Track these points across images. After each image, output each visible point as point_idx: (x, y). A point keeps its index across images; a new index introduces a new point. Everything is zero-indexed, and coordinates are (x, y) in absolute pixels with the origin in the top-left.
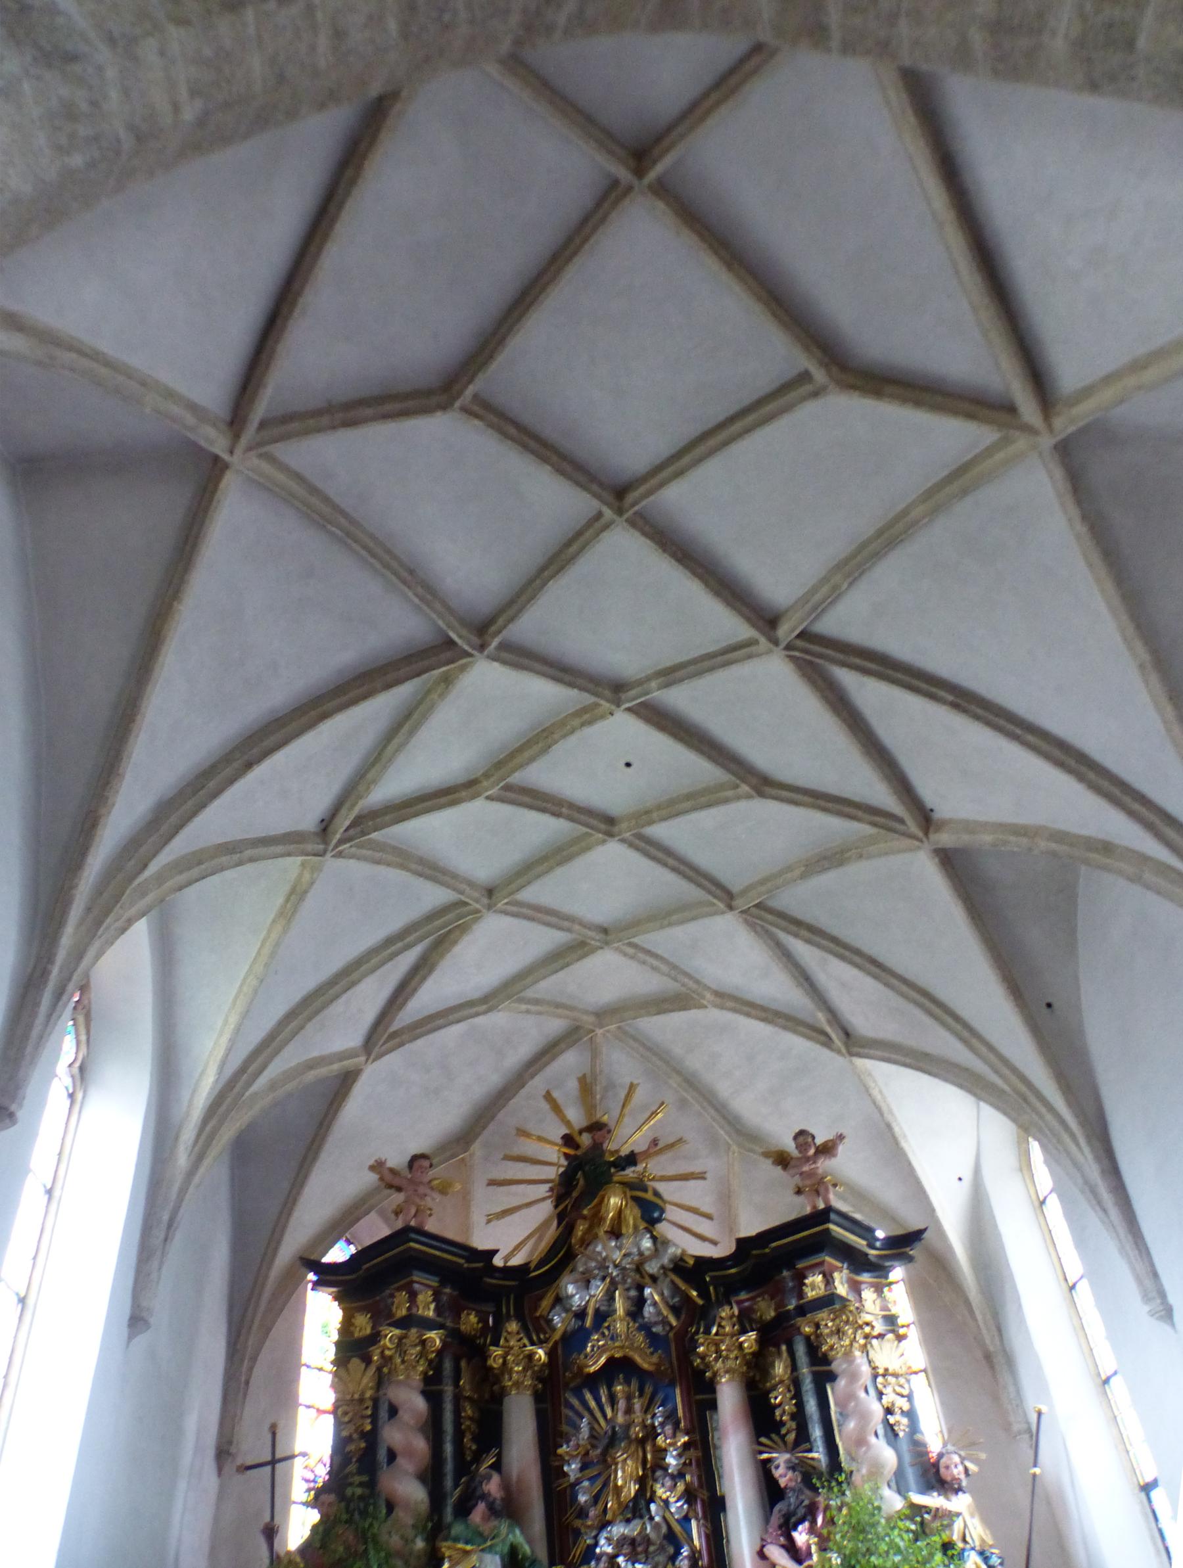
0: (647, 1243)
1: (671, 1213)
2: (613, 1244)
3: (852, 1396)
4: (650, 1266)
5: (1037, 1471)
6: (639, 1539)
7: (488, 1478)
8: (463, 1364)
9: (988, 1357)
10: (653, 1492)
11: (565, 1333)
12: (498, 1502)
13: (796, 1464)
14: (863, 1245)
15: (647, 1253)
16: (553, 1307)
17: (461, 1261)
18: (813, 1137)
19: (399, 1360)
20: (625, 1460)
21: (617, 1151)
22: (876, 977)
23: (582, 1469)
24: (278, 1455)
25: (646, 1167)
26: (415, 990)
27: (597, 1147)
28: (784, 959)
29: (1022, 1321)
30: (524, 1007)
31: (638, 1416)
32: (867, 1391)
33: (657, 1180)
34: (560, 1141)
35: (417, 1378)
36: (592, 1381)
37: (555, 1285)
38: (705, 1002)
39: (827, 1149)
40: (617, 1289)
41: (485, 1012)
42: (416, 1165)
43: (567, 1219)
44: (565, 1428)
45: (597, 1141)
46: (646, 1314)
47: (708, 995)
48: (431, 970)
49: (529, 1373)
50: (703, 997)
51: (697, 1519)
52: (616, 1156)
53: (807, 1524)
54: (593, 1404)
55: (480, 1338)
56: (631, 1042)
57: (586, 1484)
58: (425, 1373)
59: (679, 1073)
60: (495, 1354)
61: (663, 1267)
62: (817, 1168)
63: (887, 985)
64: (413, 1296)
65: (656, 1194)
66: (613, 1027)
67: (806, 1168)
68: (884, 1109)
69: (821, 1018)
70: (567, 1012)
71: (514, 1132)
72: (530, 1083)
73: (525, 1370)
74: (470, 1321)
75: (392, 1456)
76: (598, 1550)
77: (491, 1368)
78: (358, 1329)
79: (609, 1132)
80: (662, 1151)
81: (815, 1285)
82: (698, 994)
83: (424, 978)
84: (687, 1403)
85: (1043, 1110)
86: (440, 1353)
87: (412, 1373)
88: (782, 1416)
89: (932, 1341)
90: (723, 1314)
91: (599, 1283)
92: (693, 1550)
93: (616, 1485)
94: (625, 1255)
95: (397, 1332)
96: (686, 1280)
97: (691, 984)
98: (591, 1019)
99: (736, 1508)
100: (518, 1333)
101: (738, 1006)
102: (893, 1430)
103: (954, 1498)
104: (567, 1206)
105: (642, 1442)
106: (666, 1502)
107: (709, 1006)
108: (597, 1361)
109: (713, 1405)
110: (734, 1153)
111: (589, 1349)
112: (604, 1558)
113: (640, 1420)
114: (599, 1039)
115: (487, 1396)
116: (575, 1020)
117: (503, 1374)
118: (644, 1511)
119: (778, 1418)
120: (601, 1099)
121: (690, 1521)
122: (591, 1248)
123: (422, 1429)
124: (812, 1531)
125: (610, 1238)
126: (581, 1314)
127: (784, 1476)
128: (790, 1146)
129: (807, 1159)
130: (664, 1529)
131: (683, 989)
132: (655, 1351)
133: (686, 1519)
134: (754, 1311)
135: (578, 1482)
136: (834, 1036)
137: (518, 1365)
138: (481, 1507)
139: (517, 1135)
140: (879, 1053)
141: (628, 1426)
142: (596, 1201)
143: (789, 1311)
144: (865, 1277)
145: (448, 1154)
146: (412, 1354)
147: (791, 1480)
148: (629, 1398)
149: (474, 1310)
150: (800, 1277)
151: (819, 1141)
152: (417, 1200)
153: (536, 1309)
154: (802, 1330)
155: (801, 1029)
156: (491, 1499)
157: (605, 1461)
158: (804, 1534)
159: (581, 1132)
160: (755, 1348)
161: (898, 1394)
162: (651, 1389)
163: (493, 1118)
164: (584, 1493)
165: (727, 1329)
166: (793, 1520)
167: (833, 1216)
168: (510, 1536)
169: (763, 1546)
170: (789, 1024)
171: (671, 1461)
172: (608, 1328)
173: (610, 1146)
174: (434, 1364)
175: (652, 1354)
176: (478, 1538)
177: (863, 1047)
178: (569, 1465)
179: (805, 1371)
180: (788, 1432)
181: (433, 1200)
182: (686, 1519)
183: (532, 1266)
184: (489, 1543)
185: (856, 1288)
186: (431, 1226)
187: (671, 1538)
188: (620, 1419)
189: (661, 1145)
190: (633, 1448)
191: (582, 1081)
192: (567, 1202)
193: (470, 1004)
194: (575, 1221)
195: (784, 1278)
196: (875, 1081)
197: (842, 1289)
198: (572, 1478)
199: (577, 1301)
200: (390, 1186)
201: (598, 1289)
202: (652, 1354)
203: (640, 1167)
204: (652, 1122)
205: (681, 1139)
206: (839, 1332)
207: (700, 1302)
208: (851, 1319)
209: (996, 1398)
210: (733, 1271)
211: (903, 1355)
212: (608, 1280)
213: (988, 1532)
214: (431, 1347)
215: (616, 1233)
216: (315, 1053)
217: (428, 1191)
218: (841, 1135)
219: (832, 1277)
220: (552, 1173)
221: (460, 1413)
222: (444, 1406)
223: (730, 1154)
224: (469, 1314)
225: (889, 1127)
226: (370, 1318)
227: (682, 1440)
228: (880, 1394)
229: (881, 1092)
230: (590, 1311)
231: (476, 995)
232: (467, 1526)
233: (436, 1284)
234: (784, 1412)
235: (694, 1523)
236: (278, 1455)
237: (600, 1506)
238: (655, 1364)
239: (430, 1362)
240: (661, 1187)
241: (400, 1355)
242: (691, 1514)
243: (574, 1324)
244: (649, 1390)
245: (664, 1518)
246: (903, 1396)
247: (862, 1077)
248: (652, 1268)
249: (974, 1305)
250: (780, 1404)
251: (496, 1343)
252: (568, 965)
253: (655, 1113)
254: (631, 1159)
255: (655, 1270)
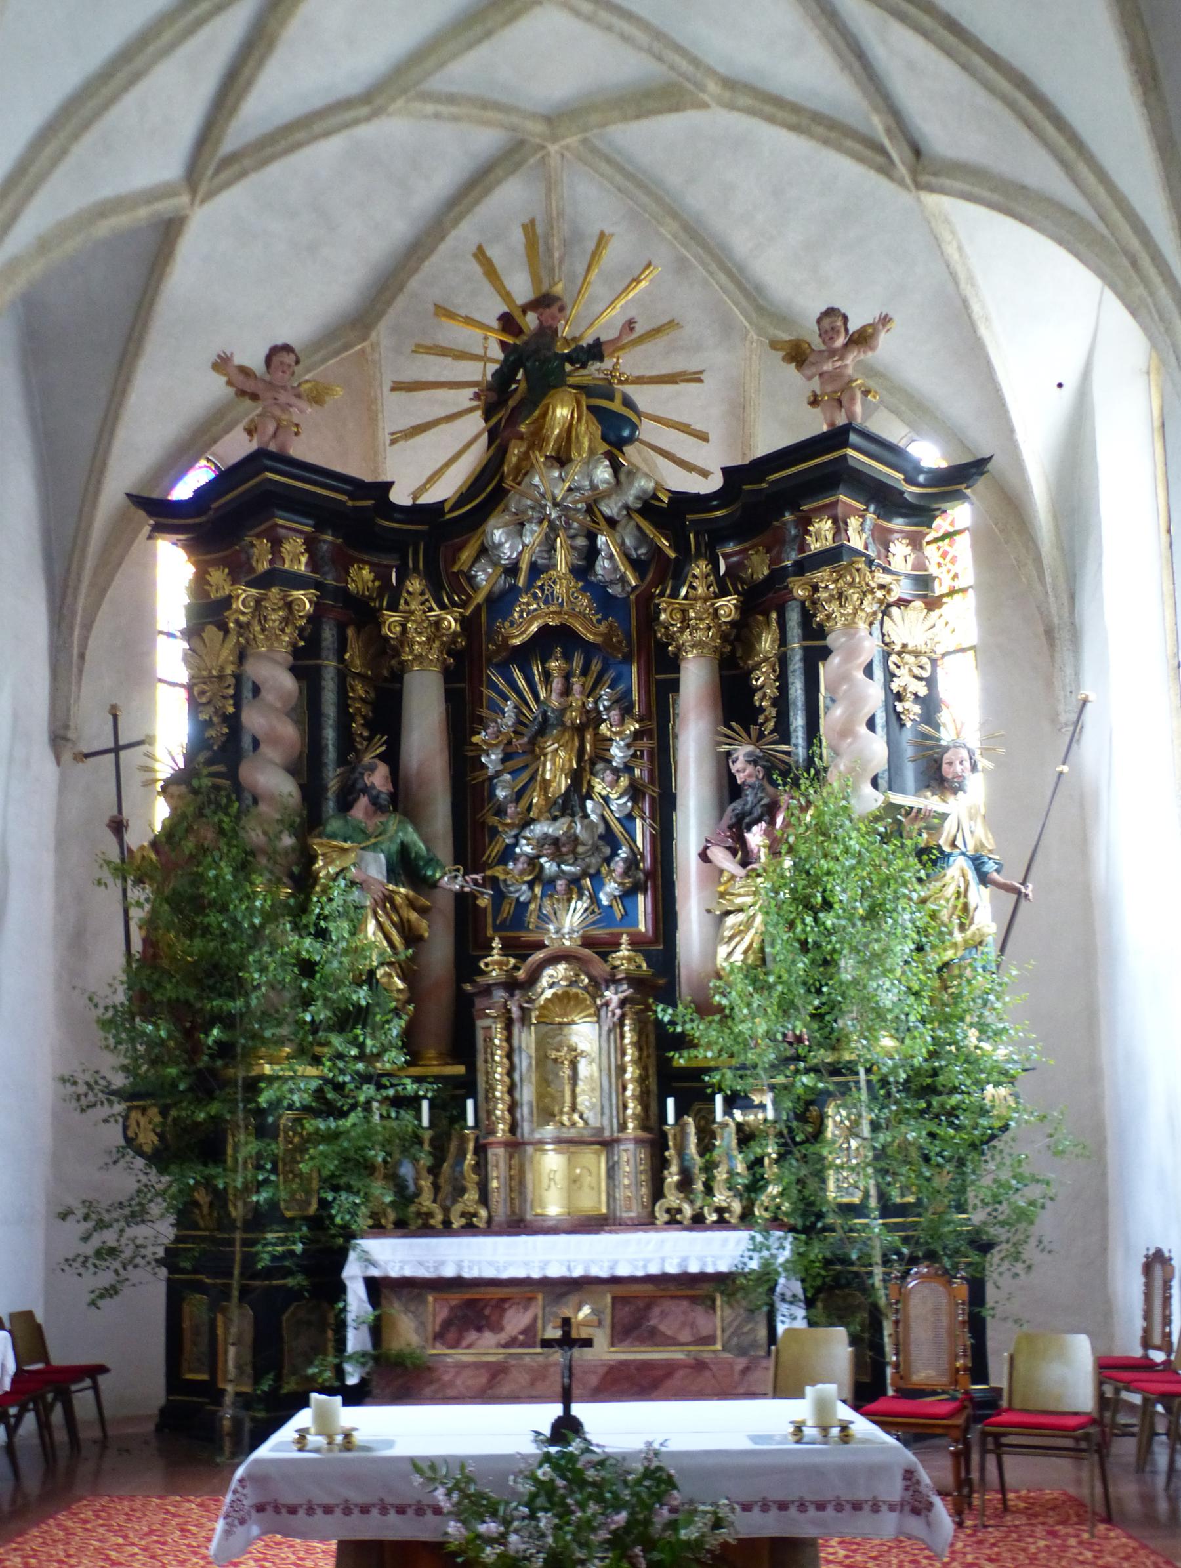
0: (603, 473)
1: (648, 430)
2: (556, 474)
3: (846, 677)
4: (608, 506)
5: (1065, 769)
6: (564, 839)
7: (372, 769)
8: (350, 632)
9: (1050, 633)
10: (591, 787)
11: (490, 593)
12: (383, 796)
13: (759, 757)
14: (898, 480)
15: (603, 487)
16: (476, 559)
17: (343, 498)
18: (845, 319)
19: (258, 628)
20: (557, 750)
21: (574, 339)
22: (949, 52)
23: (503, 761)
24: (122, 742)
25: (617, 363)
26: (249, 83)
27: (547, 333)
28: (823, 21)
29: (1098, 585)
30: (430, 108)
31: (576, 699)
32: (869, 671)
33: (633, 383)
34: (495, 324)
35: (282, 648)
36: (524, 655)
37: (480, 530)
38: (706, 97)
39: (862, 339)
40: (558, 536)
41: (368, 119)
42: (276, 360)
43: (498, 441)
44: (485, 712)
45: (545, 324)
46: (599, 570)
47: (712, 86)
48: (271, 45)
49: (437, 644)
50: (702, 88)
51: (643, 819)
52: (573, 346)
53: (763, 825)
54: (522, 683)
55: (374, 600)
56: (604, 167)
57: (507, 777)
58: (294, 645)
59: (675, 215)
60: (392, 619)
61: (626, 507)
62: (846, 366)
63: (965, 67)
64: (276, 544)
65: (628, 402)
66: (572, 140)
67: (828, 367)
68: (962, 276)
69: (877, 125)
70: (499, 116)
71: (431, 308)
72: (454, 233)
73: (430, 640)
74: (362, 578)
75: (256, 744)
76: (518, 850)
77: (387, 639)
78: (214, 588)
79: (562, 309)
80: (642, 339)
81: (821, 535)
82: (695, 84)
83: (260, 64)
84: (645, 685)
85: (1157, 280)
86: (315, 619)
87: (276, 645)
88: (761, 701)
89: (988, 612)
90: (697, 572)
91: (536, 528)
92: (633, 850)
93: (544, 780)
94: (570, 490)
95: (253, 592)
96: (659, 526)
97: (684, 65)
98: (538, 127)
99: (687, 807)
100: (422, 593)
101: (757, 105)
102: (899, 719)
103: (951, 799)
104: (500, 420)
105: (580, 730)
106: (606, 799)
107: (713, 104)
108: (526, 630)
109: (674, 686)
110: (752, 343)
111: (516, 615)
112: (522, 859)
113: (580, 703)
114: (555, 161)
115: (385, 673)
116: (514, 129)
117: (402, 645)
118: (578, 809)
119: (757, 703)
120: (561, 261)
121: (635, 819)
122: (527, 479)
123: (292, 713)
124: (768, 833)
125: (552, 467)
126: (512, 570)
127: (742, 770)
128: (811, 335)
129: (832, 353)
130: (601, 829)
131: (673, 76)
132: (605, 618)
133: (630, 817)
134: (745, 568)
135: (498, 774)
136: (895, 156)
137: (420, 634)
138: (364, 801)
139: (436, 314)
140: (958, 185)
141: (562, 711)
142: (537, 413)
143: (786, 567)
144: (898, 524)
145: (339, 344)
146: (274, 621)
147: (750, 776)
148: (567, 677)
149: (366, 562)
150: (805, 522)
151: (853, 327)
152: (278, 412)
153: (454, 561)
154: (795, 594)
155: (849, 143)
156: (374, 792)
157: (533, 751)
158: (758, 836)
159: (524, 310)
160: (734, 615)
161: (916, 677)
162: (599, 666)
163: (401, 288)
164: (503, 788)
165: (700, 591)
166: (747, 820)
167: (853, 438)
168: (400, 834)
169: (706, 848)
170: (833, 135)
171: (617, 753)
172: (541, 588)
173: (565, 331)
174: (306, 634)
175: (599, 621)
176: (362, 837)
177: (935, 174)
178: (488, 755)
179: (796, 645)
180: (767, 720)
181: (303, 413)
182: (630, 817)
183: (447, 507)
184: (373, 841)
185: (883, 539)
186: (299, 450)
187: (609, 837)
188: (555, 702)
189: (640, 329)
190: (566, 737)
191: (529, 229)
192: (499, 416)
193: (346, 104)
194: (509, 440)
195: (785, 523)
196: (953, 232)
197: (856, 541)
198: (491, 770)
199: (508, 552)
200: (241, 393)
201: (533, 535)
202: (599, 621)
203: (608, 364)
204: (631, 295)
205: (673, 320)
206: (841, 597)
207: (673, 555)
208: (857, 580)
209: (1049, 684)
210: (719, 513)
211: (934, 626)
212: (546, 523)
213: (990, 836)
214: (299, 611)
215: (561, 460)
216: (107, 191)
217: (294, 400)
218: (887, 315)
219: (846, 524)
220: (481, 372)
221: (347, 693)
222: (324, 683)
223: (748, 343)
224: (360, 569)
225: (965, 303)
226: (229, 574)
227: (632, 728)
228: (890, 676)
229: (960, 248)
230: (524, 566)
231: (353, 88)
232: (346, 821)
233: (309, 529)
234: (765, 695)
235: (638, 822)
236: (122, 742)
237: (524, 803)
238: (601, 635)
239: (301, 630)
240: (643, 397)
241: (259, 621)
242: (636, 813)
243: (502, 582)
244: (596, 666)
245: (603, 817)
246: (920, 679)
247: (933, 224)
248: (610, 508)
249: (1045, 561)
250: (762, 687)
251: (393, 607)
252: (489, 34)
253: (637, 280)
254: (596, 351)
255: (615, 511)
